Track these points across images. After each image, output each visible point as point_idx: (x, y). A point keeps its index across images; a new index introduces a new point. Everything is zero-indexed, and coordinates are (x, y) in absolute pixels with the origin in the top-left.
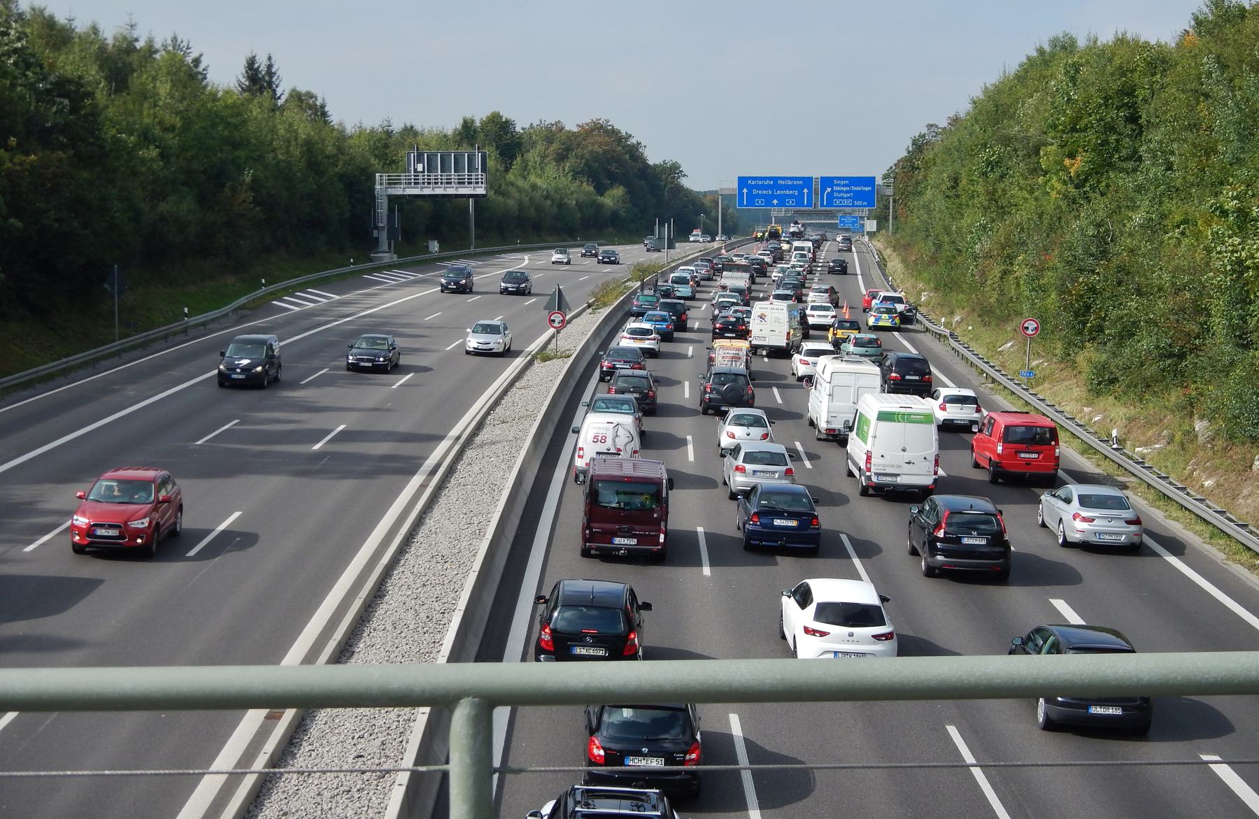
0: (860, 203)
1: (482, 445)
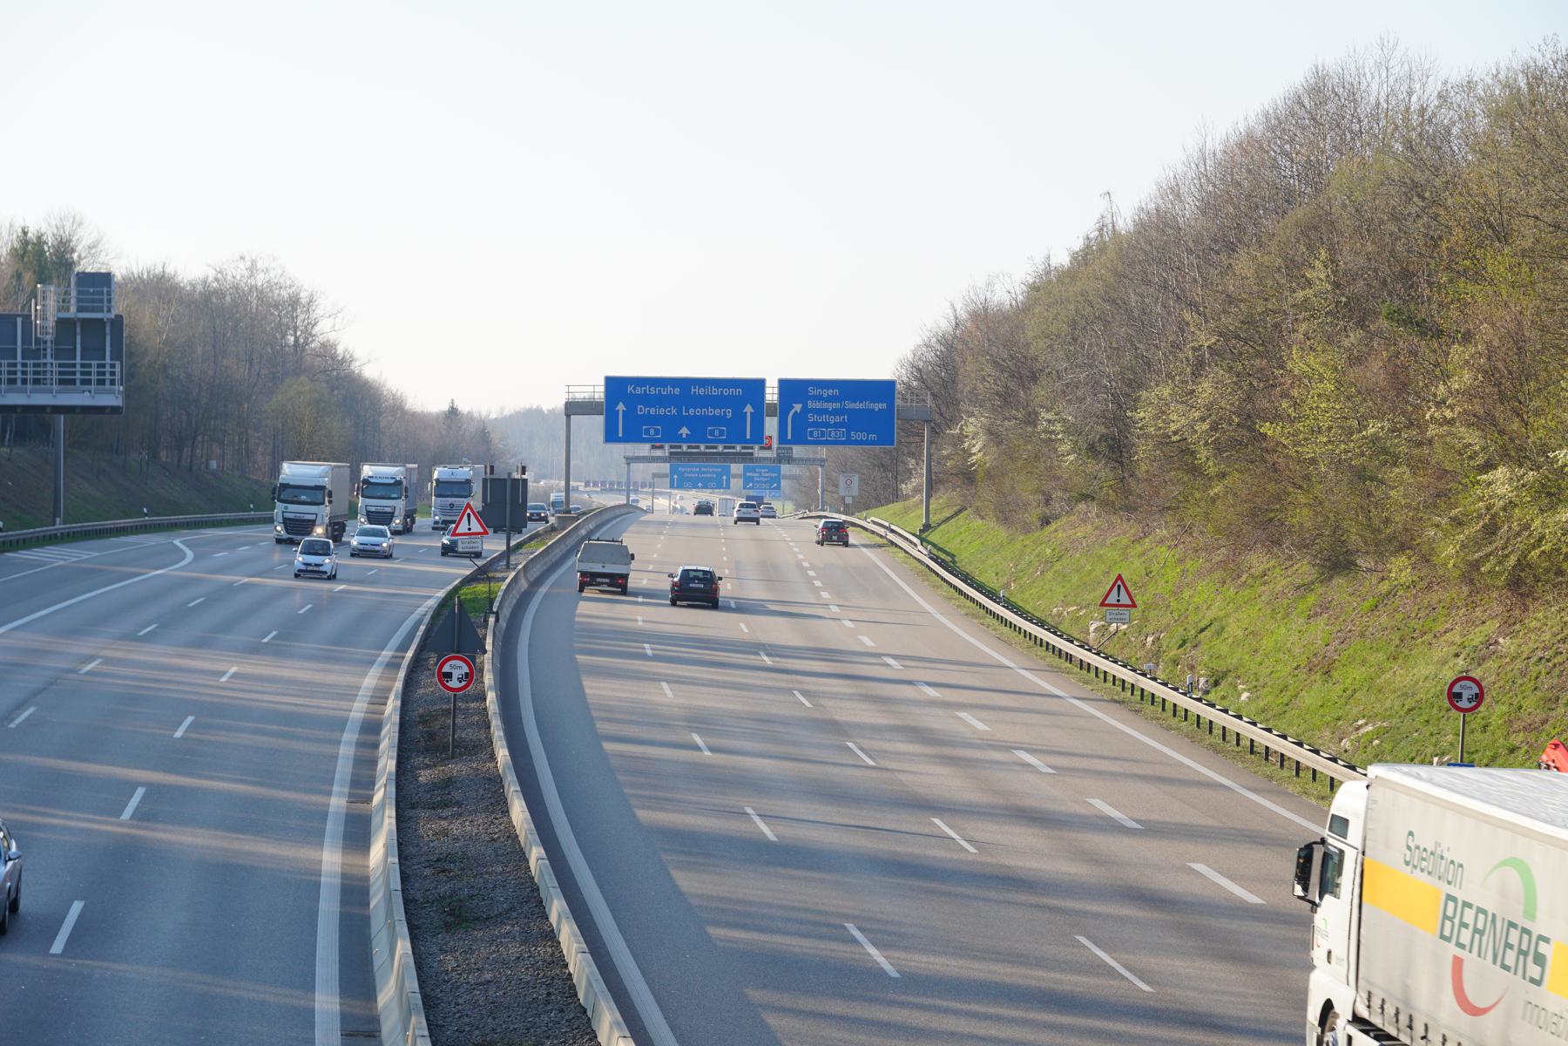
0: (862, 436)
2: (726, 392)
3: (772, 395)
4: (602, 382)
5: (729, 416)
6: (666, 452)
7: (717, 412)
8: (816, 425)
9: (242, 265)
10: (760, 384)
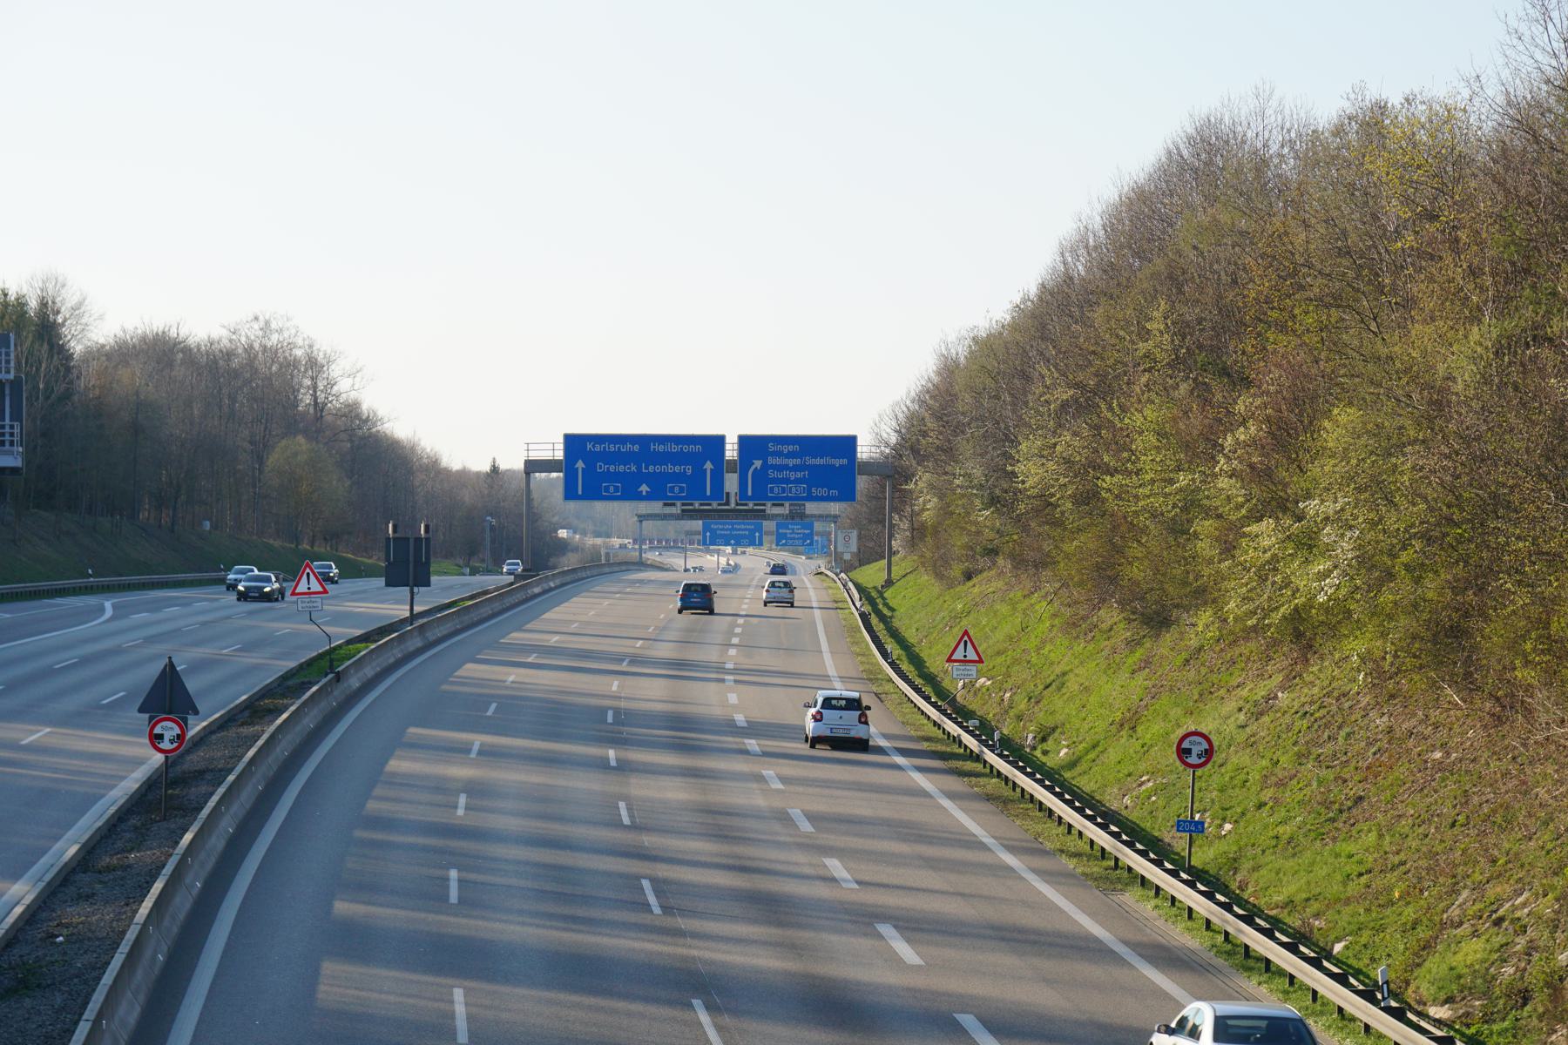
0: (823, 492)
1: (474, 710)
2: (686, 448)
3: (731, 452)
4: (561, 440)
5: (689, 472)
6: (676, 510)
7: (677, 469)
8: (774, 481)
9: (256, 326)
10: (719, 441)
